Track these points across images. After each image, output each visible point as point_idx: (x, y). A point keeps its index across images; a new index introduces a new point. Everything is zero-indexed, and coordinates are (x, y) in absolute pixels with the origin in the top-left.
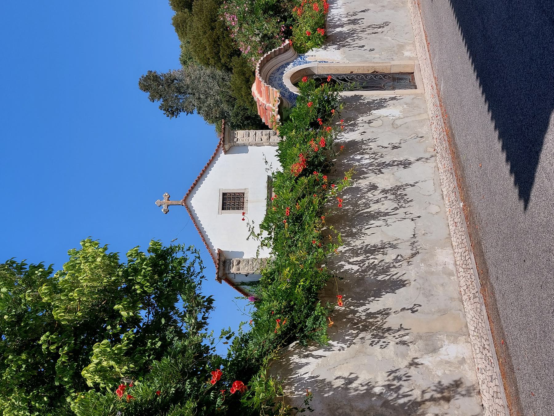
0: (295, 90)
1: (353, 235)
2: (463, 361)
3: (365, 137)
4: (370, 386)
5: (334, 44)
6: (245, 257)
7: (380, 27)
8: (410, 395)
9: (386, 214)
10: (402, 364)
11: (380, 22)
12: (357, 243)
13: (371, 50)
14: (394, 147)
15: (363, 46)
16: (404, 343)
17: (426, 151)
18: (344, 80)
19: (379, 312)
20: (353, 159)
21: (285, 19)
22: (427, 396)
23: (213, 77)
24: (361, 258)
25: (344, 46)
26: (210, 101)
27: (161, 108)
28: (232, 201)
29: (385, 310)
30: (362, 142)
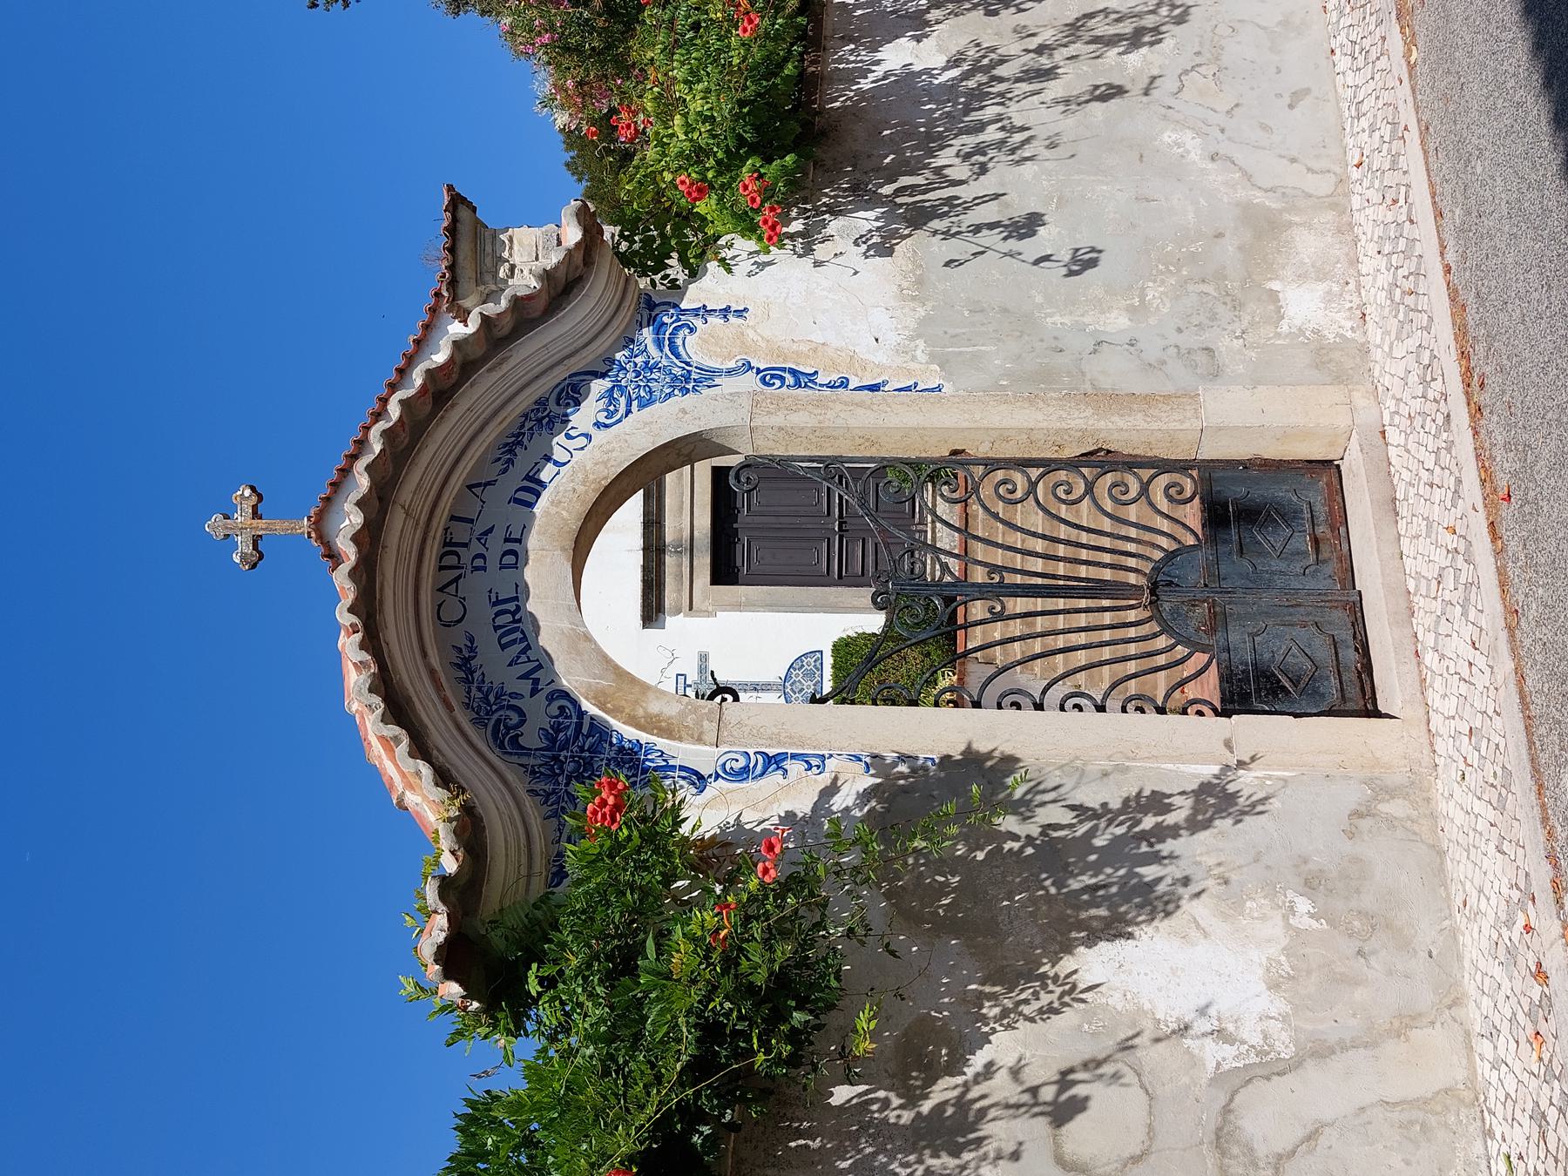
5: (862, 196)
7: (1135, 40)
13: (1083, 262)
15: (1028, 225)
25: (918, 217)
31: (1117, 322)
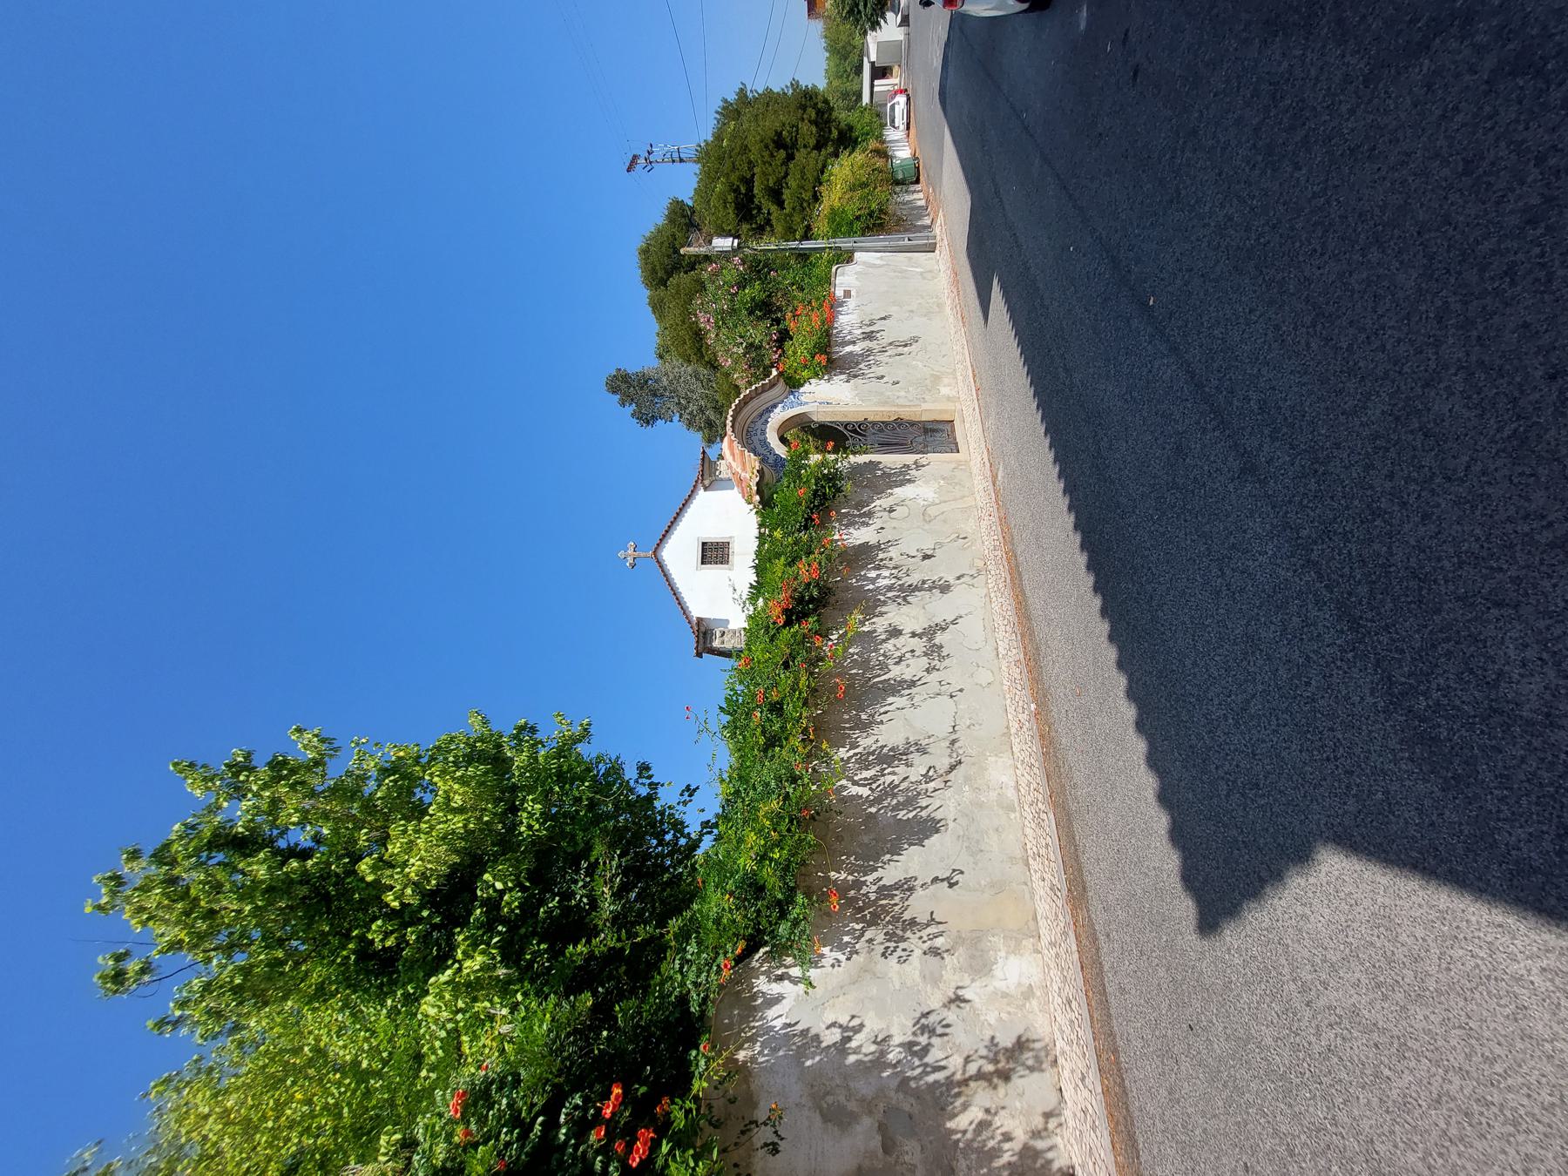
0: (781, 450)
1: (864, 727)
2: (1029, 993)
3: (884, 537)
4: (882, 1042)
6: (731, 627)
8: (944, 1068)
9: (913, 684)
10: (935, 1000)
11: (904, 337)
12: (866, 742)
14: (926, 557)
16: (935, 952)
17: (972, 566)
18: (855, 431)
19: (897, 886)
20: (866, 578)
21: (778, 321)
22: (972, 1069)
23: (696, 376)
24: (872, 773)
26: (693, 408)
27: (633, 415)
28: (713, 553)
29: (907, 880)
30: (878, 547)
31: (902, 393)
